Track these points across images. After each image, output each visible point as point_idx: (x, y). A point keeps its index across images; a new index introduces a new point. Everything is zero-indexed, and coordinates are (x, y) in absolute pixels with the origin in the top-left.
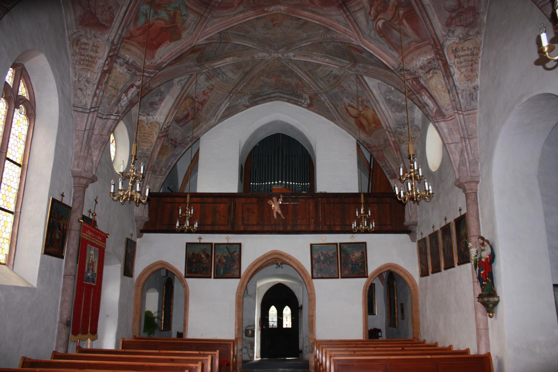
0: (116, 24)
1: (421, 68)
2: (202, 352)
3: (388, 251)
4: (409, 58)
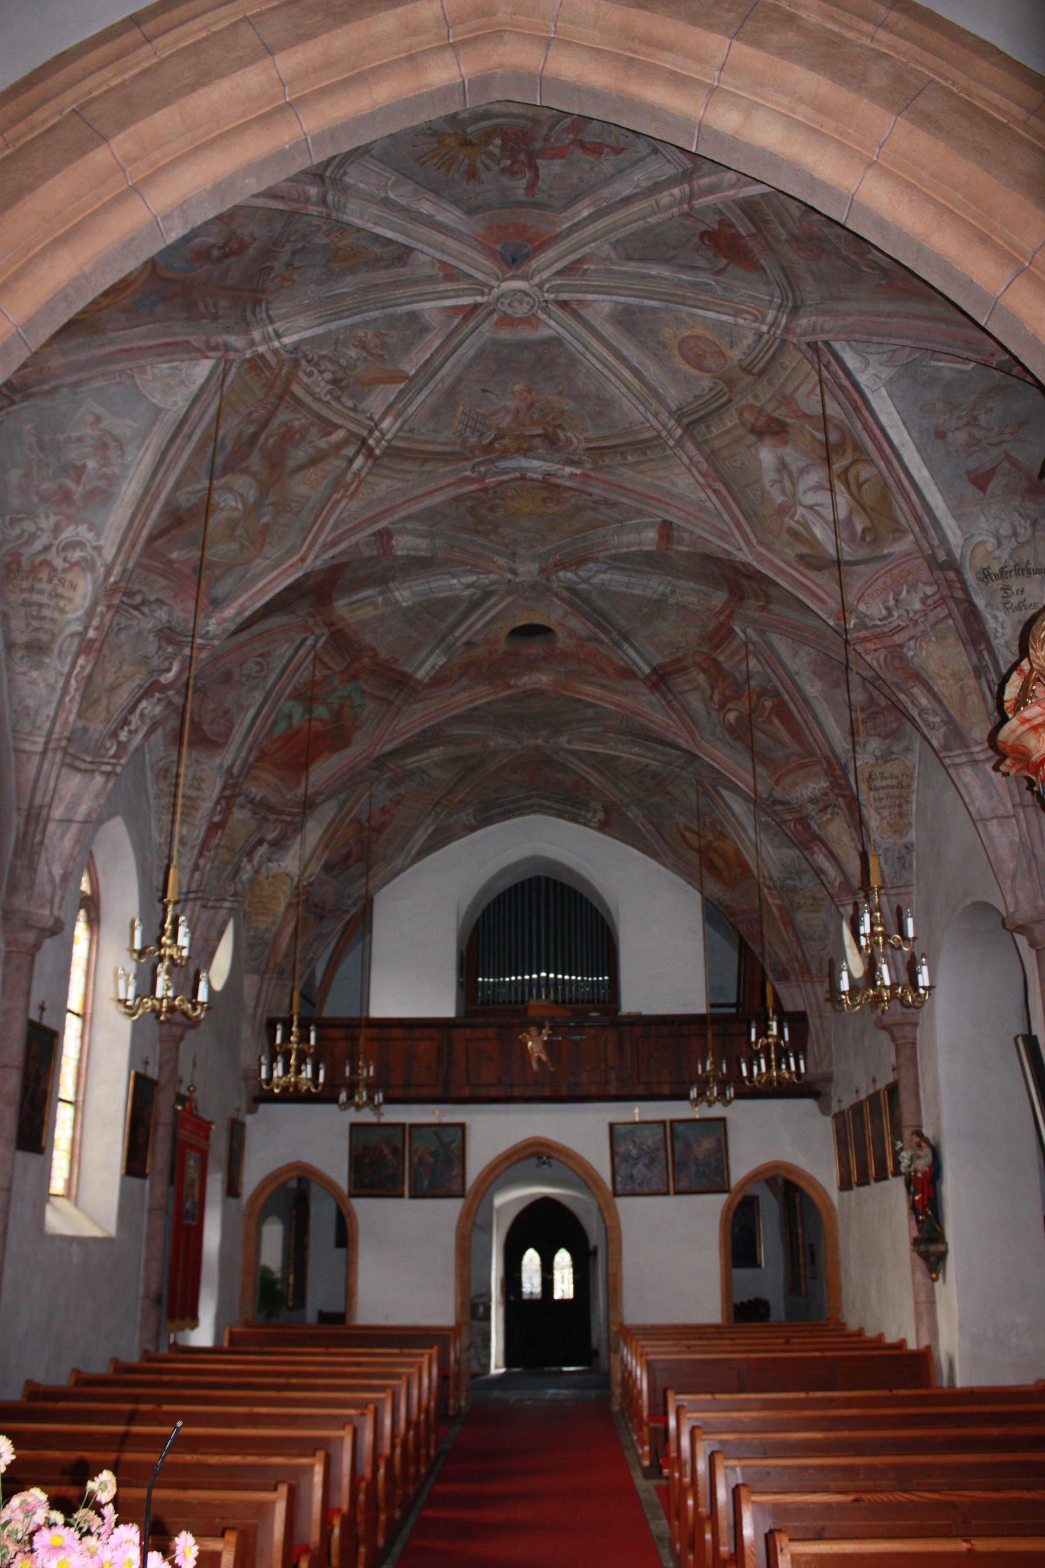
0: (236, 739)
1: (811, 801)
2: (406, 1351)
3: (768, 1136)
4: (788, 780)
